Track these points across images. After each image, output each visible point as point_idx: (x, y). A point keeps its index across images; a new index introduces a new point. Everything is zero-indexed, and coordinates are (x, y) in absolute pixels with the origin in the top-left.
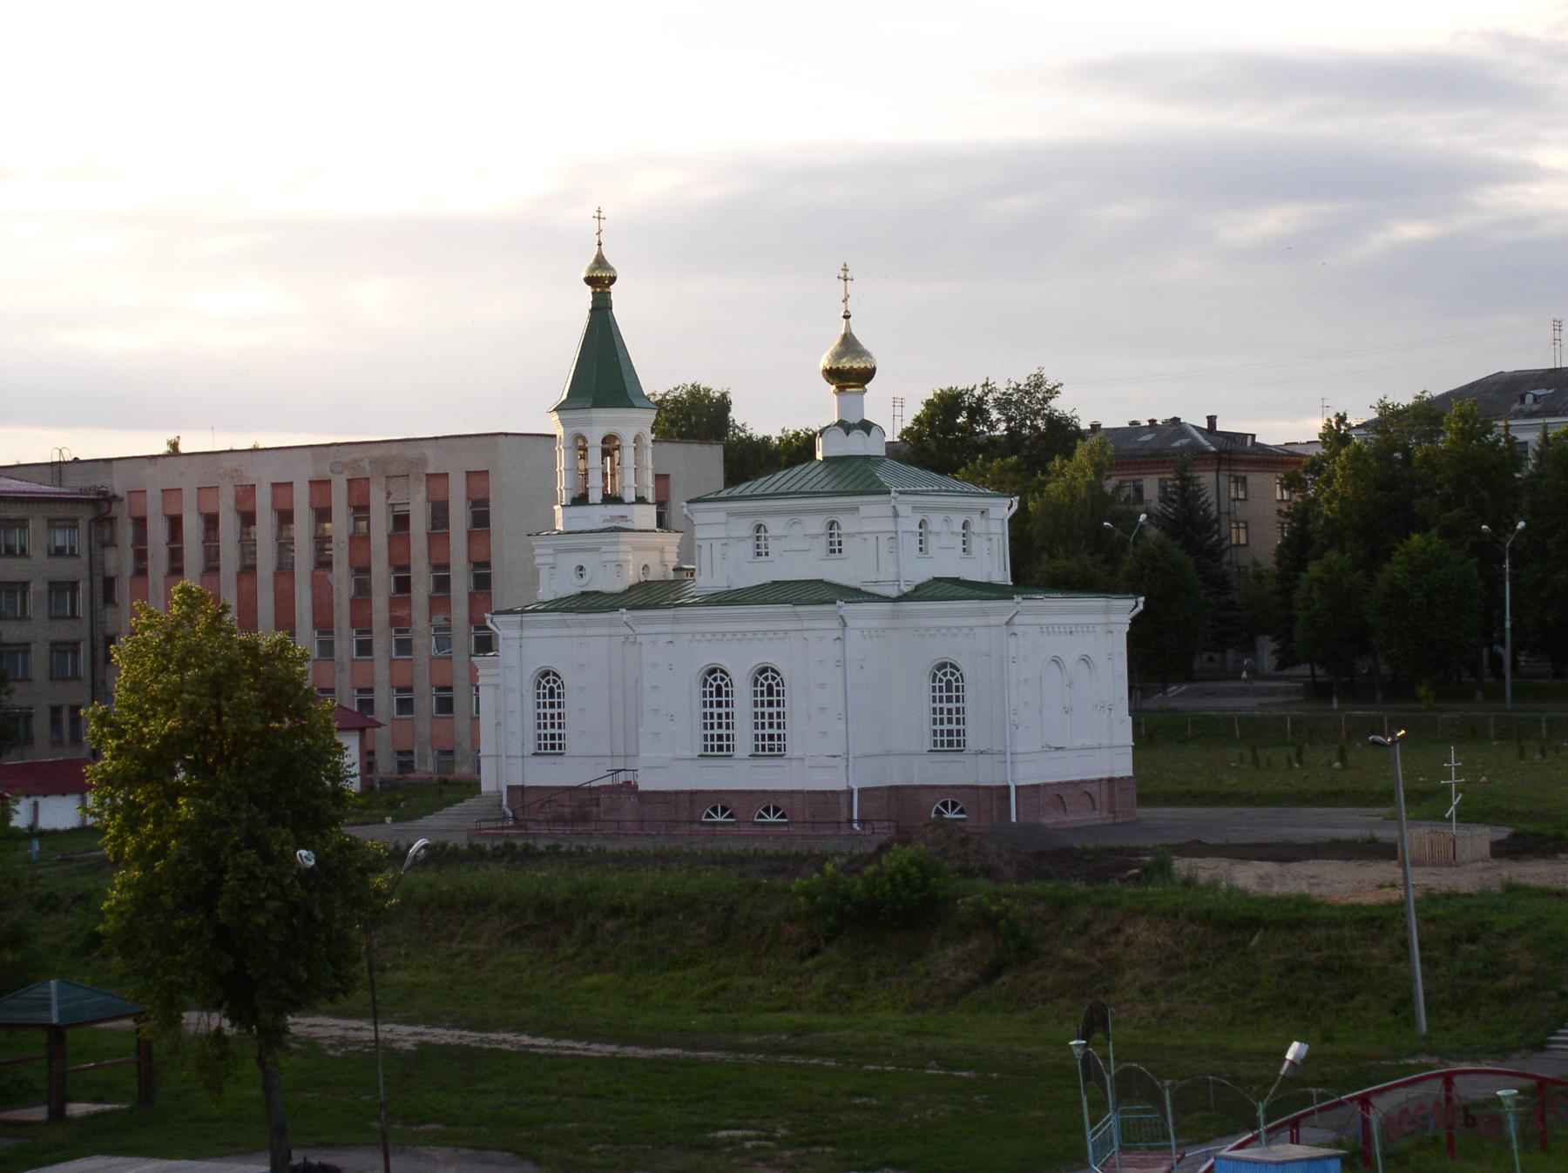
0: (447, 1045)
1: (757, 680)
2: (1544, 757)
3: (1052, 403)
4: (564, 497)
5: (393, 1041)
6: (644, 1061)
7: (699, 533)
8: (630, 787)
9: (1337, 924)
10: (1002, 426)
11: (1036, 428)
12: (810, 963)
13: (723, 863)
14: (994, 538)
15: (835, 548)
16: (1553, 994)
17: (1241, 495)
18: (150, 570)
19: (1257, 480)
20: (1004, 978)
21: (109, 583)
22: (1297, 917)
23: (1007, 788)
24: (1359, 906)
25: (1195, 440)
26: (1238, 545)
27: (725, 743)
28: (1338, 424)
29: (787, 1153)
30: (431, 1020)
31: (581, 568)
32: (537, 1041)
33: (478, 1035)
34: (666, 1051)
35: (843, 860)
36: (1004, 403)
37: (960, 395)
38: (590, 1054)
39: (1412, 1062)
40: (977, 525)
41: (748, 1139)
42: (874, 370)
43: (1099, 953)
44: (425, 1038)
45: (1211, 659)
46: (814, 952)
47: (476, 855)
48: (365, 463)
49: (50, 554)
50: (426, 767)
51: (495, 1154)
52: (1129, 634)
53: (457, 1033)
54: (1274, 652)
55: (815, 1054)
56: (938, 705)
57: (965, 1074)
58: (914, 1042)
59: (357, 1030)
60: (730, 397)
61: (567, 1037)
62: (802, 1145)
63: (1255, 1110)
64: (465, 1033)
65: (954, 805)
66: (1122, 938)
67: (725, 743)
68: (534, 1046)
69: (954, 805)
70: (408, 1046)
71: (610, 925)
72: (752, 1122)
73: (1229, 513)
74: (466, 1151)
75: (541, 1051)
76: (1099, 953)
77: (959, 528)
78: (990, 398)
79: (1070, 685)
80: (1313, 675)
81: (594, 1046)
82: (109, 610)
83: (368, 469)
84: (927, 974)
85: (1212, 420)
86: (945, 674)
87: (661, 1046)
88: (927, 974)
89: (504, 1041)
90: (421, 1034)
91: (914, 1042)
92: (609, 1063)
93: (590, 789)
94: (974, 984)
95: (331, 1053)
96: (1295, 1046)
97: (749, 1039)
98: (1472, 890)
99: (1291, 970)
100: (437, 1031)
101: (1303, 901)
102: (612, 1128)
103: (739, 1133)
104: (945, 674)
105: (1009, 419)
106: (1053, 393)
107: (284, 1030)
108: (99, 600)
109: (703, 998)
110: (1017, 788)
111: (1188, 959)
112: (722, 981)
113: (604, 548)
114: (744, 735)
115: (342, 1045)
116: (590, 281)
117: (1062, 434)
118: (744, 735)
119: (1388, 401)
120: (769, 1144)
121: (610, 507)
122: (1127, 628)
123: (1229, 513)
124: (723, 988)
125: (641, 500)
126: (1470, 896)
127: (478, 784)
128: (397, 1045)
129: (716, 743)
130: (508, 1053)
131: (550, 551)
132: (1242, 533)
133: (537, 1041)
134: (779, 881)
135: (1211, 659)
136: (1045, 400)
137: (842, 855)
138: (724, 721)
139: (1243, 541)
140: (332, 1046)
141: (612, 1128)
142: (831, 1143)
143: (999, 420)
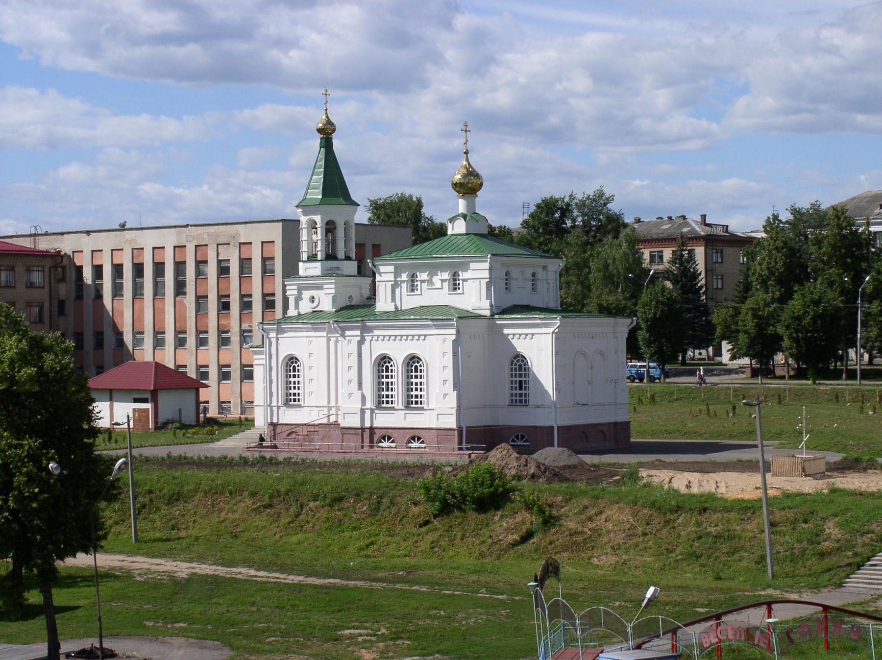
0: (207, 575)
1: (512, 362)
2: (874, 413)
3: (609, 205)
4: (305, 257)
5: (176, 572)
6: (316, 587)
7: (378, 278)
8: (336, 424)
9: (727, 510)
10: (580, 219)
11: (600, 220)
12: (423, 529)
13: (382, 469)
14: (551, 282)
15: (455, 287)
16: (850, 554)
17: (719, 260)
18: (85, 296)
19: (728, 251)
20: (535, 540)
21: (62, 303)
22: (705, 505)
23: (552, 427)
24: (743, 500)
25: (693, 229)
26: (717, 288)
27: (523, 398)
28: (774, 220)
29: (381, 644)
30: (201, 559)
31: (313, 297)
32: (258, 574)
33: (225, 569)
34: (332, 580)
35: (450, 469)
36: (582, 205)
37: (557, 201)
38: (287, 581)
39: (763, 593)
40: (541, 274)
41: (361, 635)
42: (481, 184)
43: (590, 526)
44: (194, 571)
45: (700, 354)
46: (426, 523)
47: (244, 462)
48: (205, 236)
49: (27, 287)
50: (235, 413)
51: (210, 642)
52: (627, 339)
53: (214, 567)
54: (728, 351)
55: (417, 584)
56: (514, 379)
57: (500, 597)
58: (474, 578)
59: (157, 565)
60: (423, 201)
61: (276, 571)
62: (392, 639)
63: (626, 627)
64: (219, 568)
65: (523, 437)
66: (603, 516)
67: (523, 398)
68: (256, 576)
69: (523, 437)
70: (184, 575)
71: (311, 504)
72: (367, 625)
73: (712, 270)
74: (193, 640)
75: (259, 579)
76: (590, 526)
77: (529, 276)
78: (573, 203)
79: (592, 368)
80: (751, 364)
81: (291, 577)
82: (61, 319)
83: (207, 239)
84: (491, 537)
85: (704, 217)
86: (518, 361)
87: (329, 578)
88: (491, 537)
89: (240, 573)
90: (193, 568)
91: (474, 578)
92: (298, 588)
93: (314, 425)
94: (515, 544)
95: (138, 579)
96: (652, 589)
97: (380, 575)
98: (811, 491)
99: (700, 538)
100: (203, 566)
101: (711, 497)
102: (284, 627)
103: (357, 631)
104: (518, 361)
105: (584, 215)
106: (609, 200)
107: (54, 570)
108: (56, 313)
109: (361, 549)
110: (558, 428)
111: (640, 530)
112: (372, 539)
113: (325, 286)
114: (398, 394)
115: (146, 574)
116: (320, 131)
117: (615, 224)
118: (398, 394)
119: (796, 206)
120: (373, 639)
121: (330, 262)
122: (626, 335)
123: (712, 270)
124: (372, 543)
125: (348, 258)
126: (810, 494)
127: (253, 420)
128: (176, 575)
129: (518, 398)
130: (240, 580)
131: (296, 287)
132: (720, 282)
133: (258, 574)
134: (410, 481)
135: (700, 354)
136: (605, 204)
137: (451, 466)
138: (297, 385)
139: (720, 286)
140: (139, 575)
141: (284, 627)
142: (409, 639)
143: (578, 216)
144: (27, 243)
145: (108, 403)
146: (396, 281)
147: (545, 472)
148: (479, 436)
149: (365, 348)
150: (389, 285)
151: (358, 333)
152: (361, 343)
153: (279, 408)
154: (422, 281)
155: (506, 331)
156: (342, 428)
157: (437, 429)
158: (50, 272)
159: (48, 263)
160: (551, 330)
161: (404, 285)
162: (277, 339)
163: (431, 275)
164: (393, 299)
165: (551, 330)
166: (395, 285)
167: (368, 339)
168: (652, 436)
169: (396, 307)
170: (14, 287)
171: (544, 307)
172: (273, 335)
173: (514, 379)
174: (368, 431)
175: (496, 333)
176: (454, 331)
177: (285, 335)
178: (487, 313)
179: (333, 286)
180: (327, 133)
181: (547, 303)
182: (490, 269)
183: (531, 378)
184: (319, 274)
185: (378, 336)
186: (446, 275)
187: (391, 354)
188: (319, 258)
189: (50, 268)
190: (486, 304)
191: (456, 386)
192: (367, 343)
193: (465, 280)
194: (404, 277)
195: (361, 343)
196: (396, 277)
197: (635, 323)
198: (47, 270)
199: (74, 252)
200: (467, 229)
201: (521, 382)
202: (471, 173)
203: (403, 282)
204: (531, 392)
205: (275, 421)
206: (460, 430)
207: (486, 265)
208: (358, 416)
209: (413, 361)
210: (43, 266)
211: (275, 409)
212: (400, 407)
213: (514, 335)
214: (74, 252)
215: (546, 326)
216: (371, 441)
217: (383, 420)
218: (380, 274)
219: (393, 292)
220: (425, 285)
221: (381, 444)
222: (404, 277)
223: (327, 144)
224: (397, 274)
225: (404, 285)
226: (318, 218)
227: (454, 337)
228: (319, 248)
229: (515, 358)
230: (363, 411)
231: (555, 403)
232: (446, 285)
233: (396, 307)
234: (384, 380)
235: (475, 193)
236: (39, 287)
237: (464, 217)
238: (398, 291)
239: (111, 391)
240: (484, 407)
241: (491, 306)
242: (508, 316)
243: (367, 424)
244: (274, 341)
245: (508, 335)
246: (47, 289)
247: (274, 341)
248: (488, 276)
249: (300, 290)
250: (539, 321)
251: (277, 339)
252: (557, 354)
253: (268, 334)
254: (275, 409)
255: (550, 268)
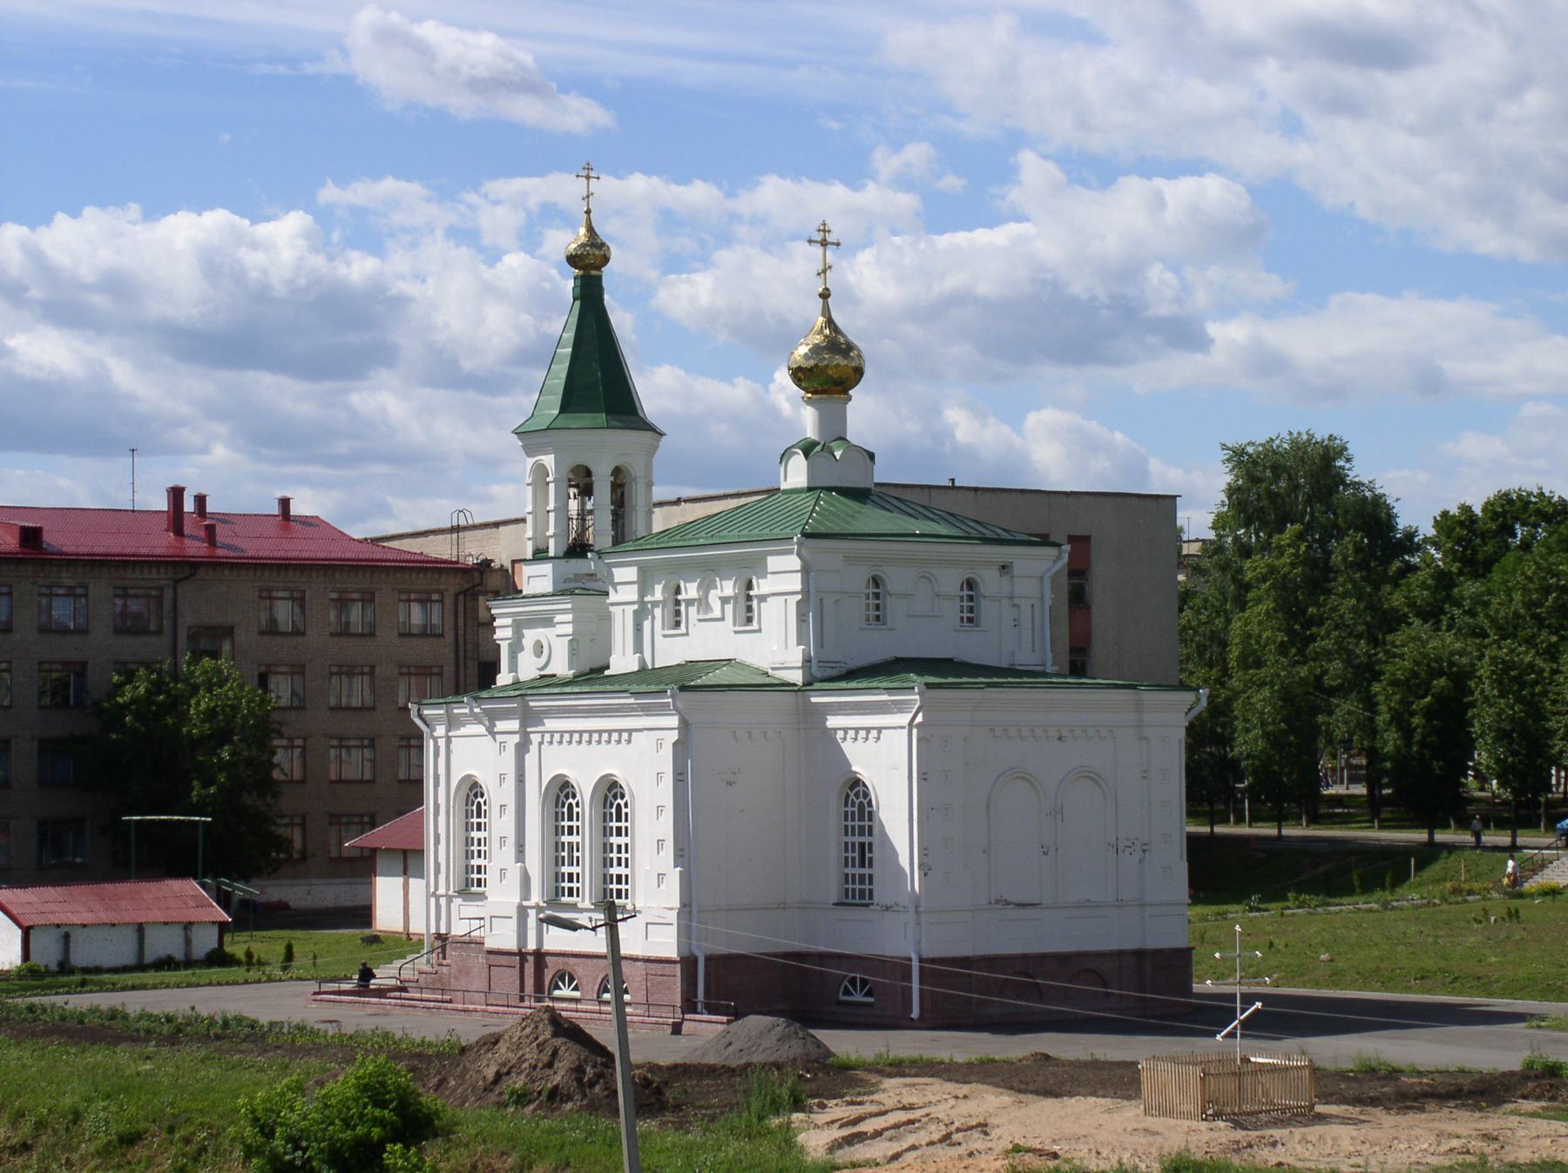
40: (991, 582)
113: (558, 618)
116: (572, 260)
144: (440, 549)
145: (400, 880)
146: (642, 603)
147: (592, 1084)
148: (718, 980)
149: (531, 759)
150: (631, 609)
151: (514, 725)
152: (522, 748)
153: (450, 899)
154: (690, 602)
155: (833, 722)
156: (490, 952)
157: (648, 960)
158: (456, 599)
159: (453, 585)
160: (904, 719)
161: (658, 612)
162: (449, 740)
163: (706, 587)
164: (638, 648)
165: (904, 719)
166: (642, 612)
167: (535, 738)
168: (1385, 985)
169: (642, 661)
170: (303, 634)
171: (1005, 665)
172: (440, 731)
173: (850, 839)
174: (531, 959)
175: (811, 725)
176: (674, 721)
177: (463, 731)
178: (796, 677)
179: (569, 617)
180: (589, 265)
181: (1013, 654)
182: (806, 571)
183: (875, 839)
184: (550, 589)
185: (552, 733)
186: (728, 588)
187: (573, 777)
188: (551, 554)
189: (457, 595)
190: (796, 655)
191: (681, 856)
192: (534, 748)
193: (763, 598)
194: (658, 593)
195: (522, 748)
196: (642, 594)
197: (1204, 702)
198: (449, 600)
199: (514, 562)
200: (811, 475)
201: (862, 845)
202: (836, 343)
203: (655, 604)
204: (876, 871)
205: (443, 931)
206: (688, 963)
207: (794, 562)
208: (513, 924)
209: (610, 791)
210: (441, 592)
211: (443, 901)
212: (587, 904)
213: (846, 730)
214: (514, 562)
215: (899, 707)
216: (539, 987)
217: (557, 940)
218: (615, 585)
219: (638, 629)
220: (693, 610)
221: (557, 993)
222: (658, 593)
223: (590, 294)
224: (644, 585)
225: (658, 612)
226: (549, 460)
227: (674, 736)
228: (551, 531)
229: (851, 788)
230: (522, 912)
231: (916, 900)
232: (729, 608)
233: (642, 661)
234: (566, 839)
235: (845, 391)
236: (362, 635)
237: (808, 449)
238: (647, 624)
239: (405, 852)
240: (782, 906)
241: (807, 661)
242: (853, 685)
243: (532, 946)
244: (442, 743)
245: (836, 730)
246: (449, 637)
247: (442, 743)
248: (798, 587)
249: (519, 627)
250: (885, 697)
251: (449, 740)
252: (923, 777)
253: (433, 730)
254: (443, 901)
255: (1018, 568)
